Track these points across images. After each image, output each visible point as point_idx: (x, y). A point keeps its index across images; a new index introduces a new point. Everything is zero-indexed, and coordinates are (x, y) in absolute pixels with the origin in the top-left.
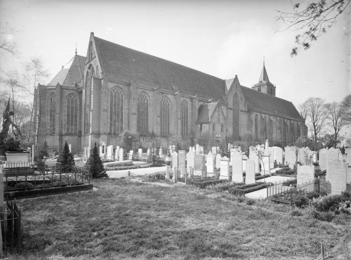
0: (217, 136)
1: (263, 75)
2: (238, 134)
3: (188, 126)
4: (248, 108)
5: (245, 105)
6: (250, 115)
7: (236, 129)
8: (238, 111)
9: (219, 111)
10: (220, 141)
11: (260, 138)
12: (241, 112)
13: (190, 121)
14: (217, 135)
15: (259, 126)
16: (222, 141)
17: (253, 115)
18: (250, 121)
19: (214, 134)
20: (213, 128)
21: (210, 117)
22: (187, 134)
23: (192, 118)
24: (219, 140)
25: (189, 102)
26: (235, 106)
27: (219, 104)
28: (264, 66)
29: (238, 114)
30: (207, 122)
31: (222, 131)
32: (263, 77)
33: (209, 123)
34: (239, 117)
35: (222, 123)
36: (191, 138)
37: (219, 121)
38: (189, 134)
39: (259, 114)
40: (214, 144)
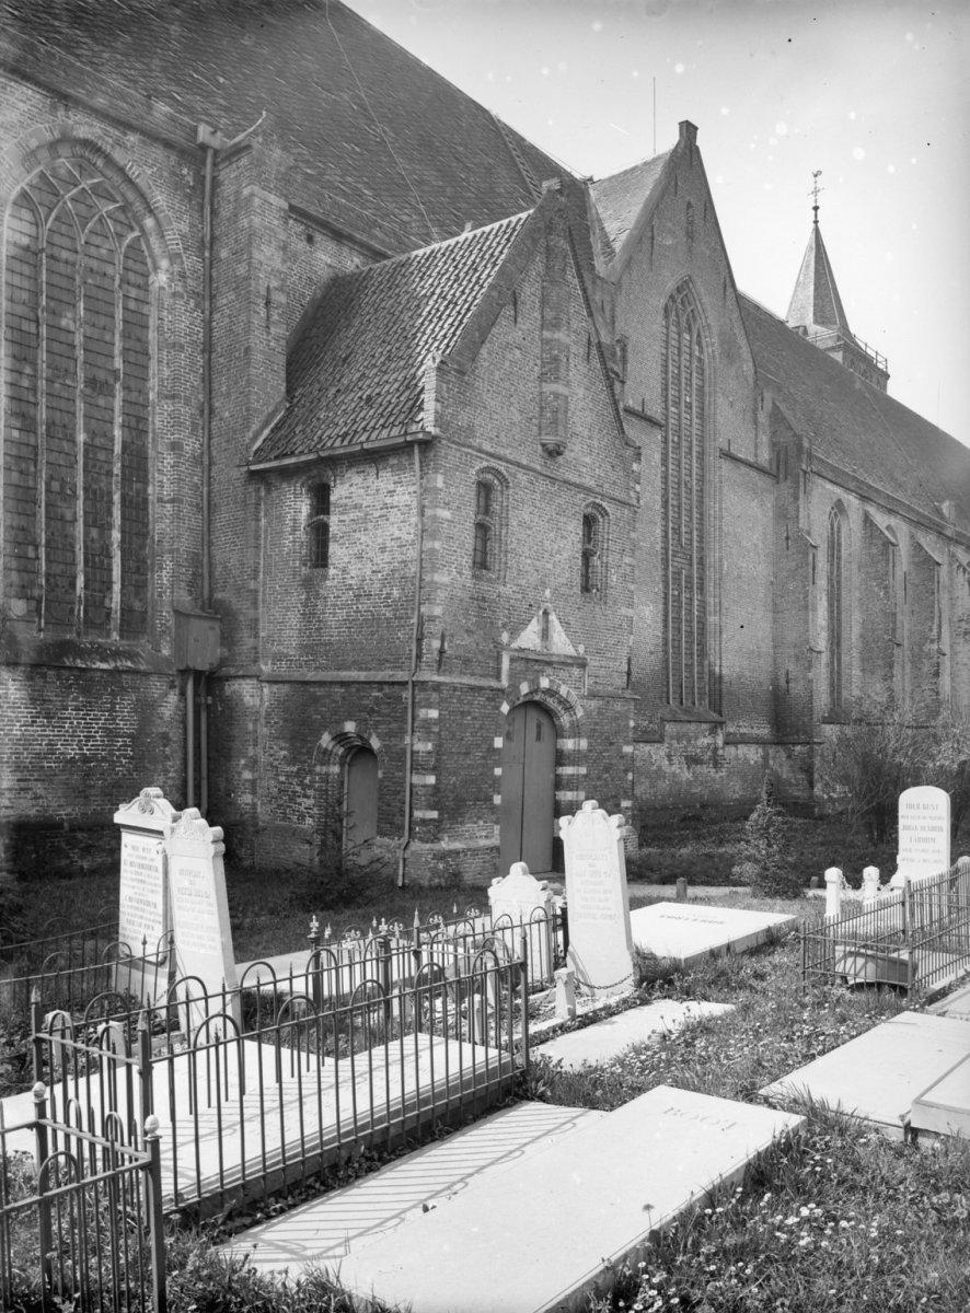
0: (529, 638)
1: (812, 288)
2: (703, 654)
3: (154, 510)
4: (774, 445)
5: (755, 411)
6: (796, 498)
7: (690, 612)
8: (701, 456)
9: (550, 314)
10: (569, 708)
11: (856, 692)
12: (726, 465)
13: (175, 447)
14: (534, 627)
15: (851, 597)
16: (593, 704)
17: (815, 500)
18: (792, 544)
19: (486, 615)
20: (482, 529)
21: (429, 382)
22: (134, 622)
23: (208, 411)
24: (551, 703)
25: (160, 199)
26: (677, 404)
27: (550, 228)
28: (817, 231)
29: (702, 479)
30: (394, 435)
31: (586, 589)
32: (812, 301)
33: (427, 444)
34: (712, 507)
35: (589, 482)
36: (198, 675)
37: (553, 453)
38: (166, 616)
39: (851, 500)
40: (498, 742)
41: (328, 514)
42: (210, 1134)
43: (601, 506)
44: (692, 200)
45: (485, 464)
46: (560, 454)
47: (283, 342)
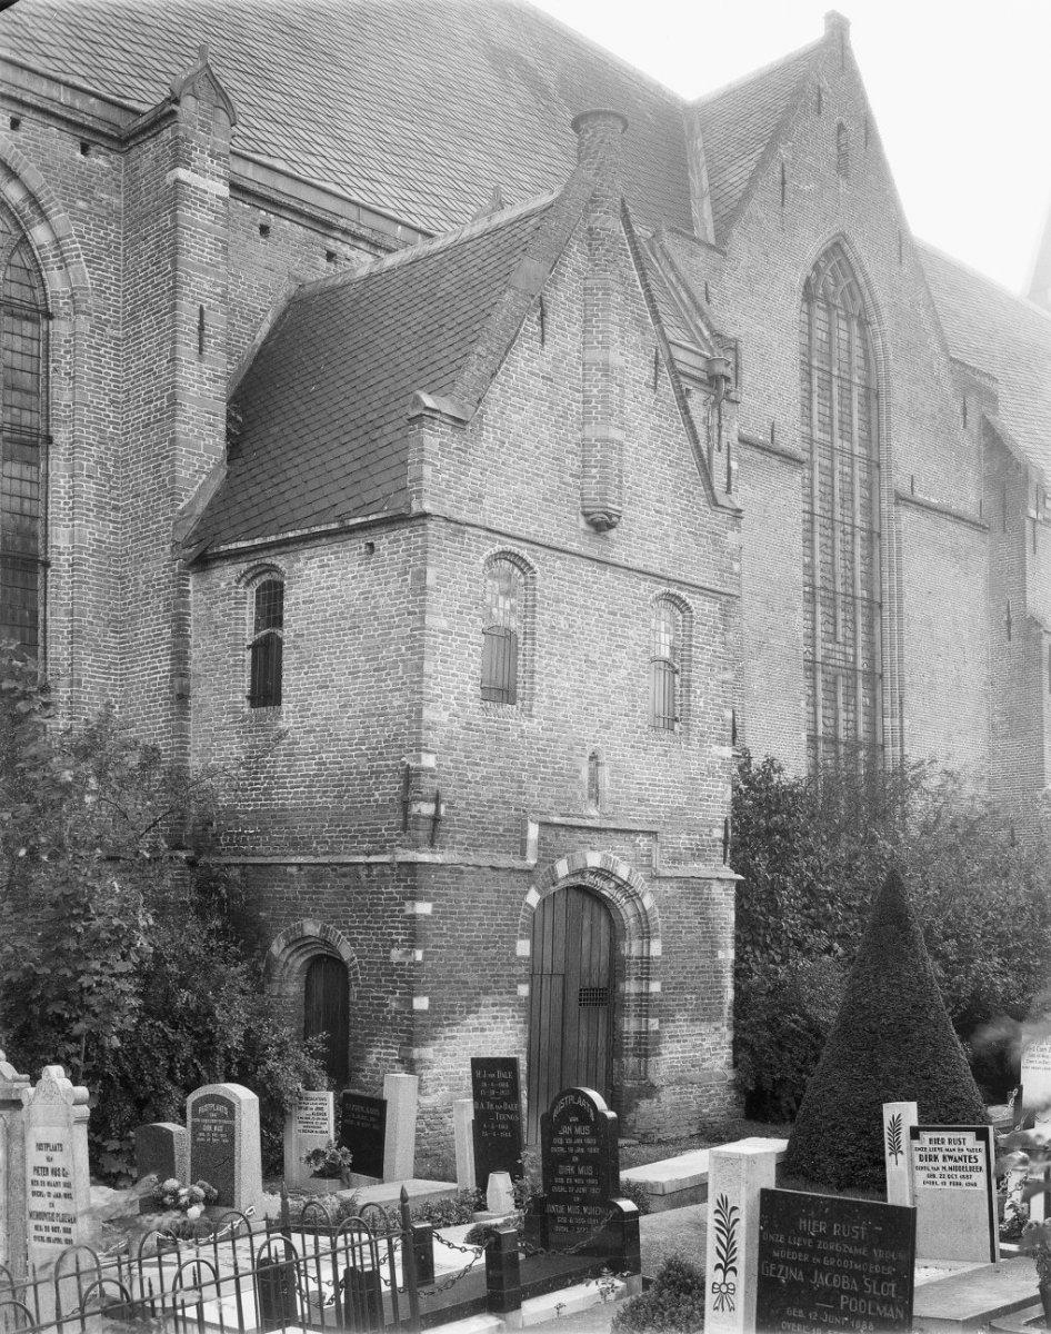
24: (608, 890)
37: (601, 525)
41: (281, 625)
42: (47, 1281)
43: (678, 598)
44: (844, 121)
45: (499, 547)
46: (611, 526)
47: (222, 384)
